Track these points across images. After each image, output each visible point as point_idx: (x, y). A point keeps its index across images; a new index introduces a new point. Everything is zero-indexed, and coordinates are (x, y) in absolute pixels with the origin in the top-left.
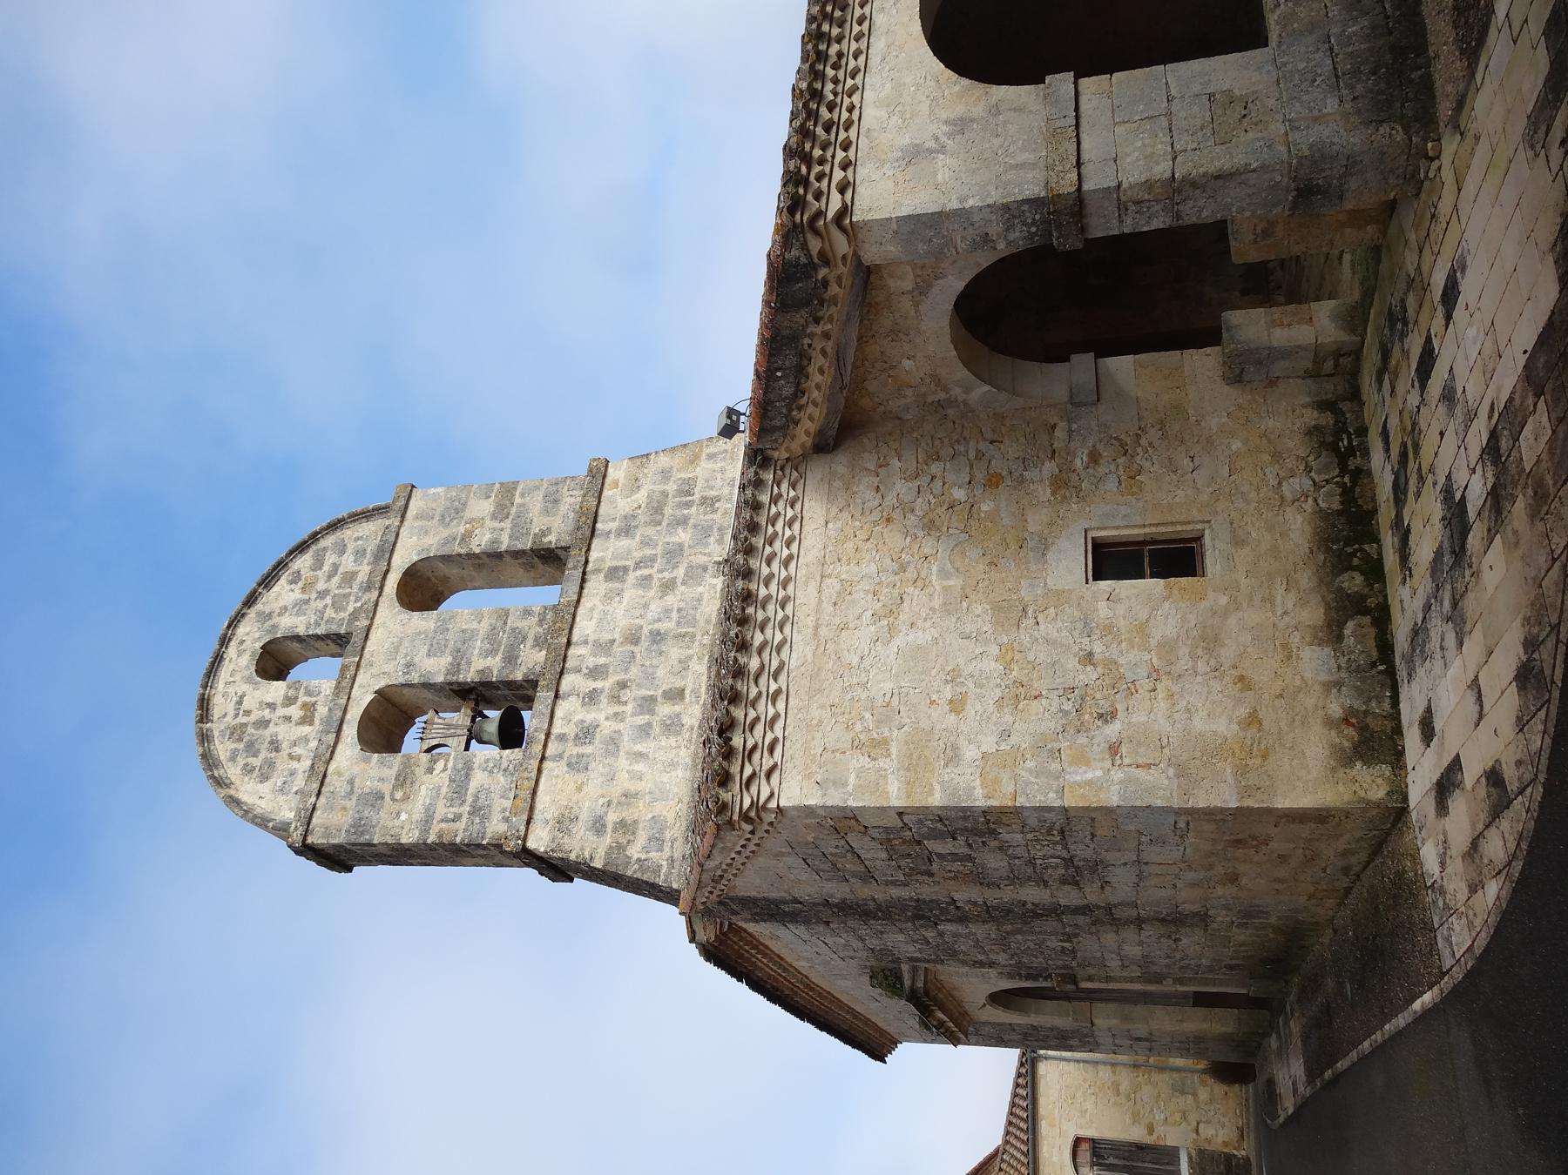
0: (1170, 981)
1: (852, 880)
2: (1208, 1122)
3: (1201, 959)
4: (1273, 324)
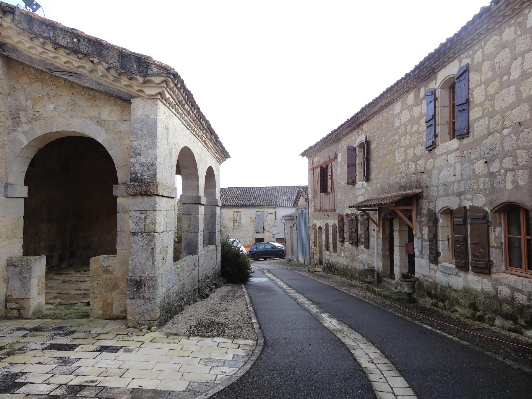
4: (40, 278)
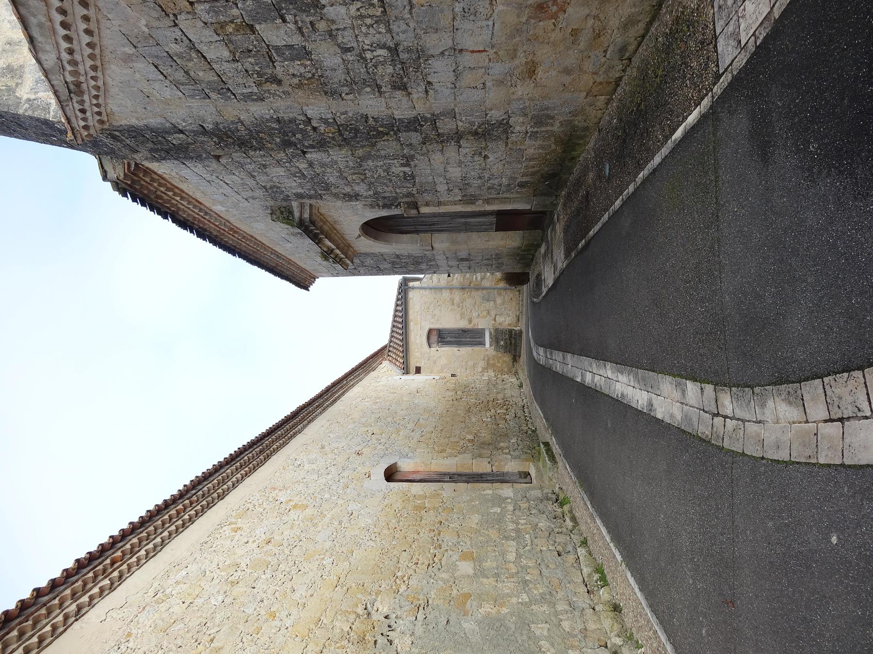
0: (480, 202)
1: (212, 95)
2: (501, 314)
3: (502, 178)
